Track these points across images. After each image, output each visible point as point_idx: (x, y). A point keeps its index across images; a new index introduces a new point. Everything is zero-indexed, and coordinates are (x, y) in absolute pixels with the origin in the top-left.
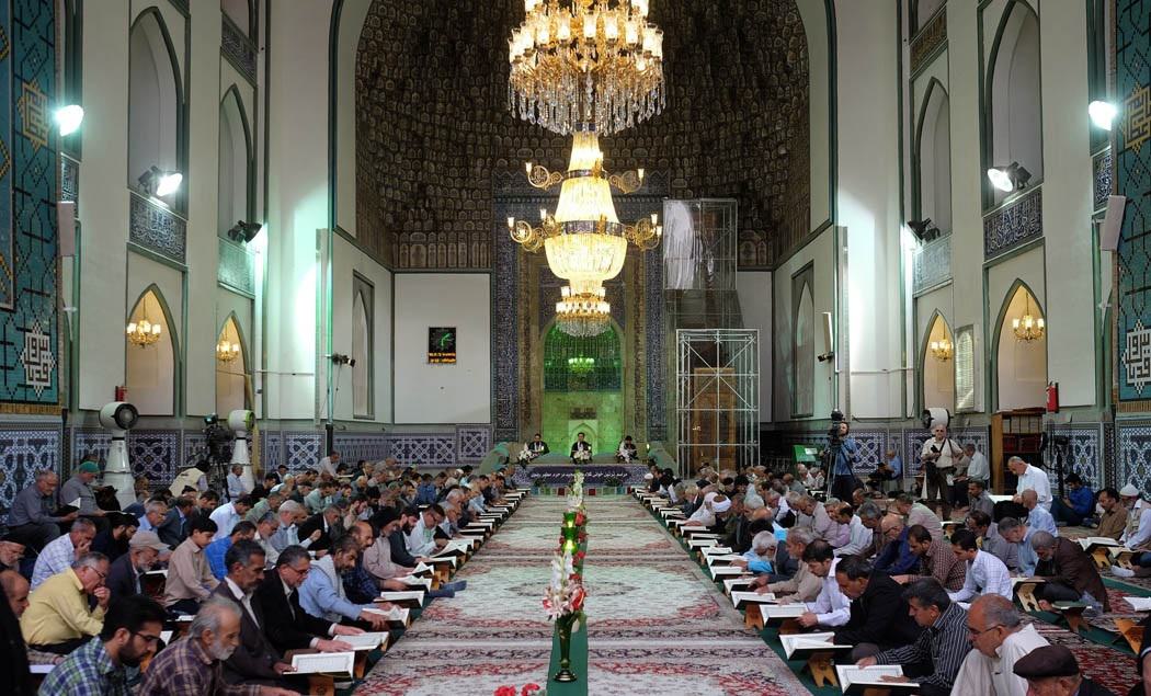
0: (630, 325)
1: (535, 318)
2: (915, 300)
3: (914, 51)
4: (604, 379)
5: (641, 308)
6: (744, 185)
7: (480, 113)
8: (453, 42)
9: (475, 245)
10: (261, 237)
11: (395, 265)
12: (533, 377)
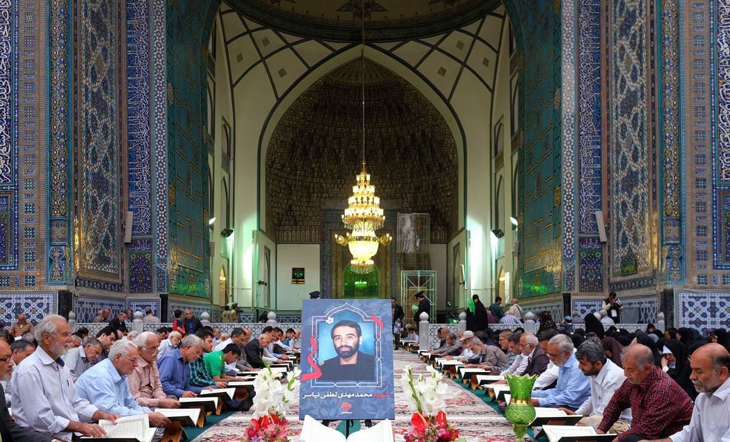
0: (383, 268)
1: (340, 263)
2: (496, 261)
3: (496, 162)
5: (388, 260)
6: (433, 206)
7: (316, 174)
8: (305, 147)
9: (313, 232)
10: (233, 235)
11: (278, 241)
12: (339, 290)
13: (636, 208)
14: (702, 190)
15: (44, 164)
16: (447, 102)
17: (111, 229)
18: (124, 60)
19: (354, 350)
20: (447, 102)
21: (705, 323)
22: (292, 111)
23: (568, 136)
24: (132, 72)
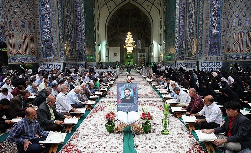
4: (131, 58)
11: (110, 47)
13: (192, 41)
14: (207, 43)
15: (58, 33)
16: (149, 13)
17: (73, 47)
18: (74, 7)
19: (129, 95)
20: (149, 13)
21: (206, 68)
22: (113, 16)
23: (177, 23)
24: (76, 10)
